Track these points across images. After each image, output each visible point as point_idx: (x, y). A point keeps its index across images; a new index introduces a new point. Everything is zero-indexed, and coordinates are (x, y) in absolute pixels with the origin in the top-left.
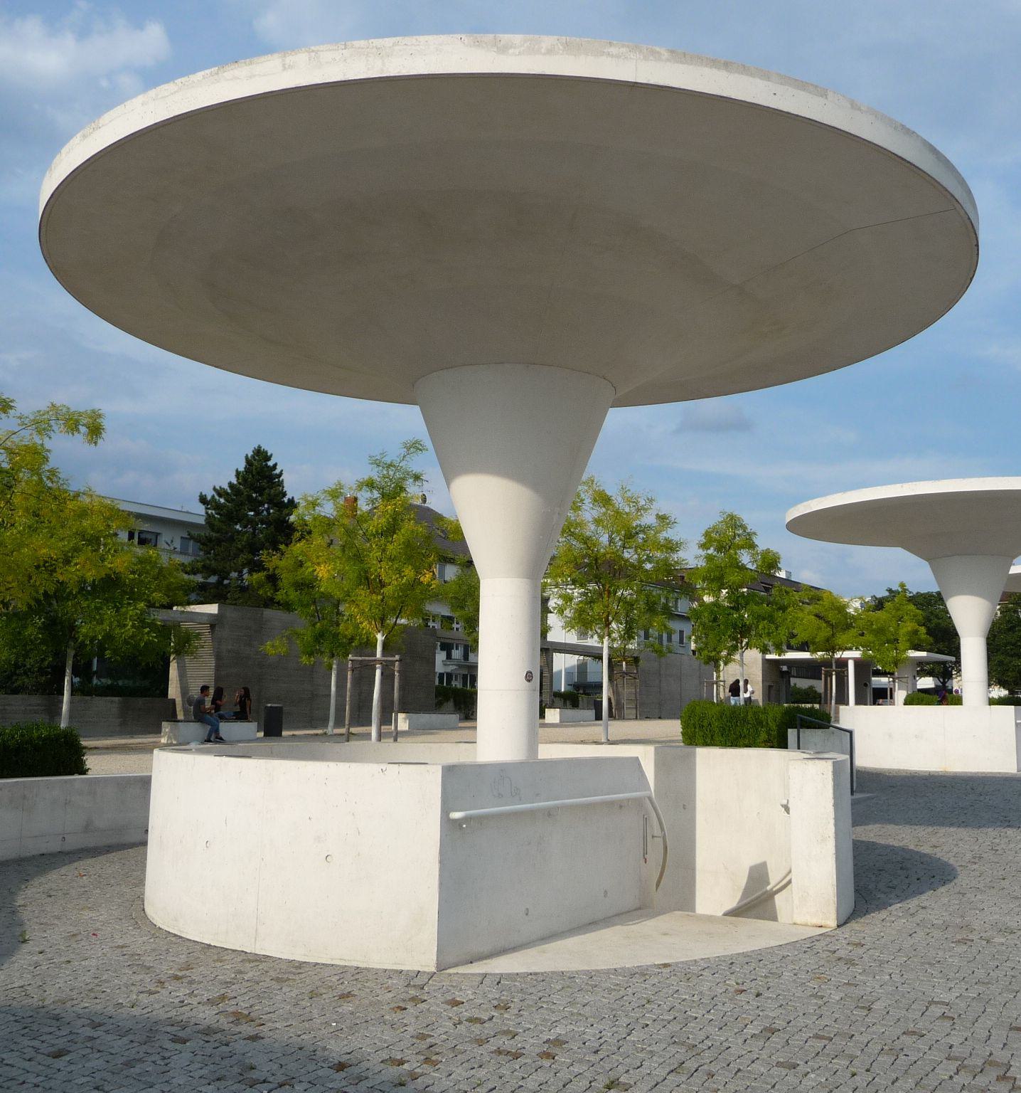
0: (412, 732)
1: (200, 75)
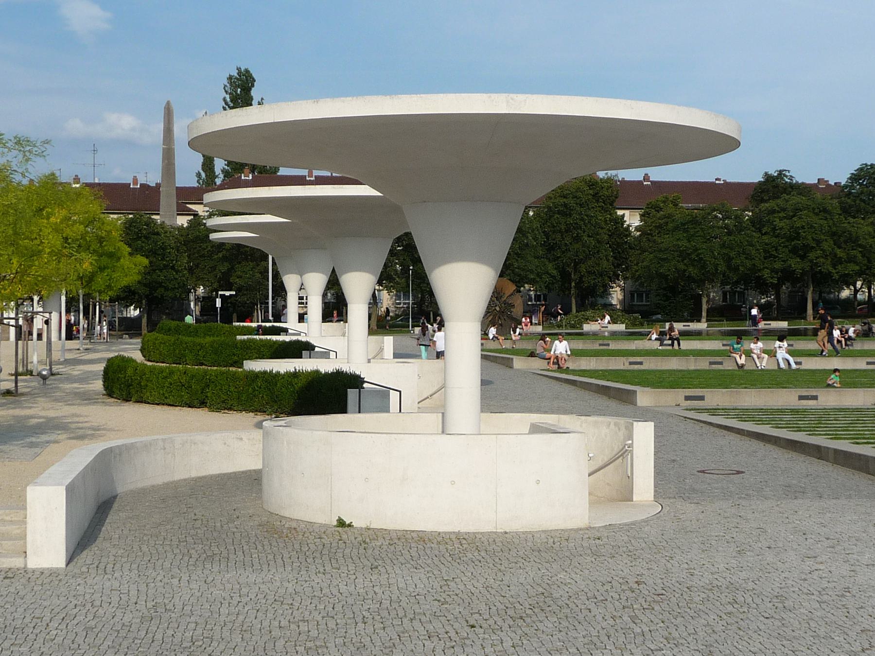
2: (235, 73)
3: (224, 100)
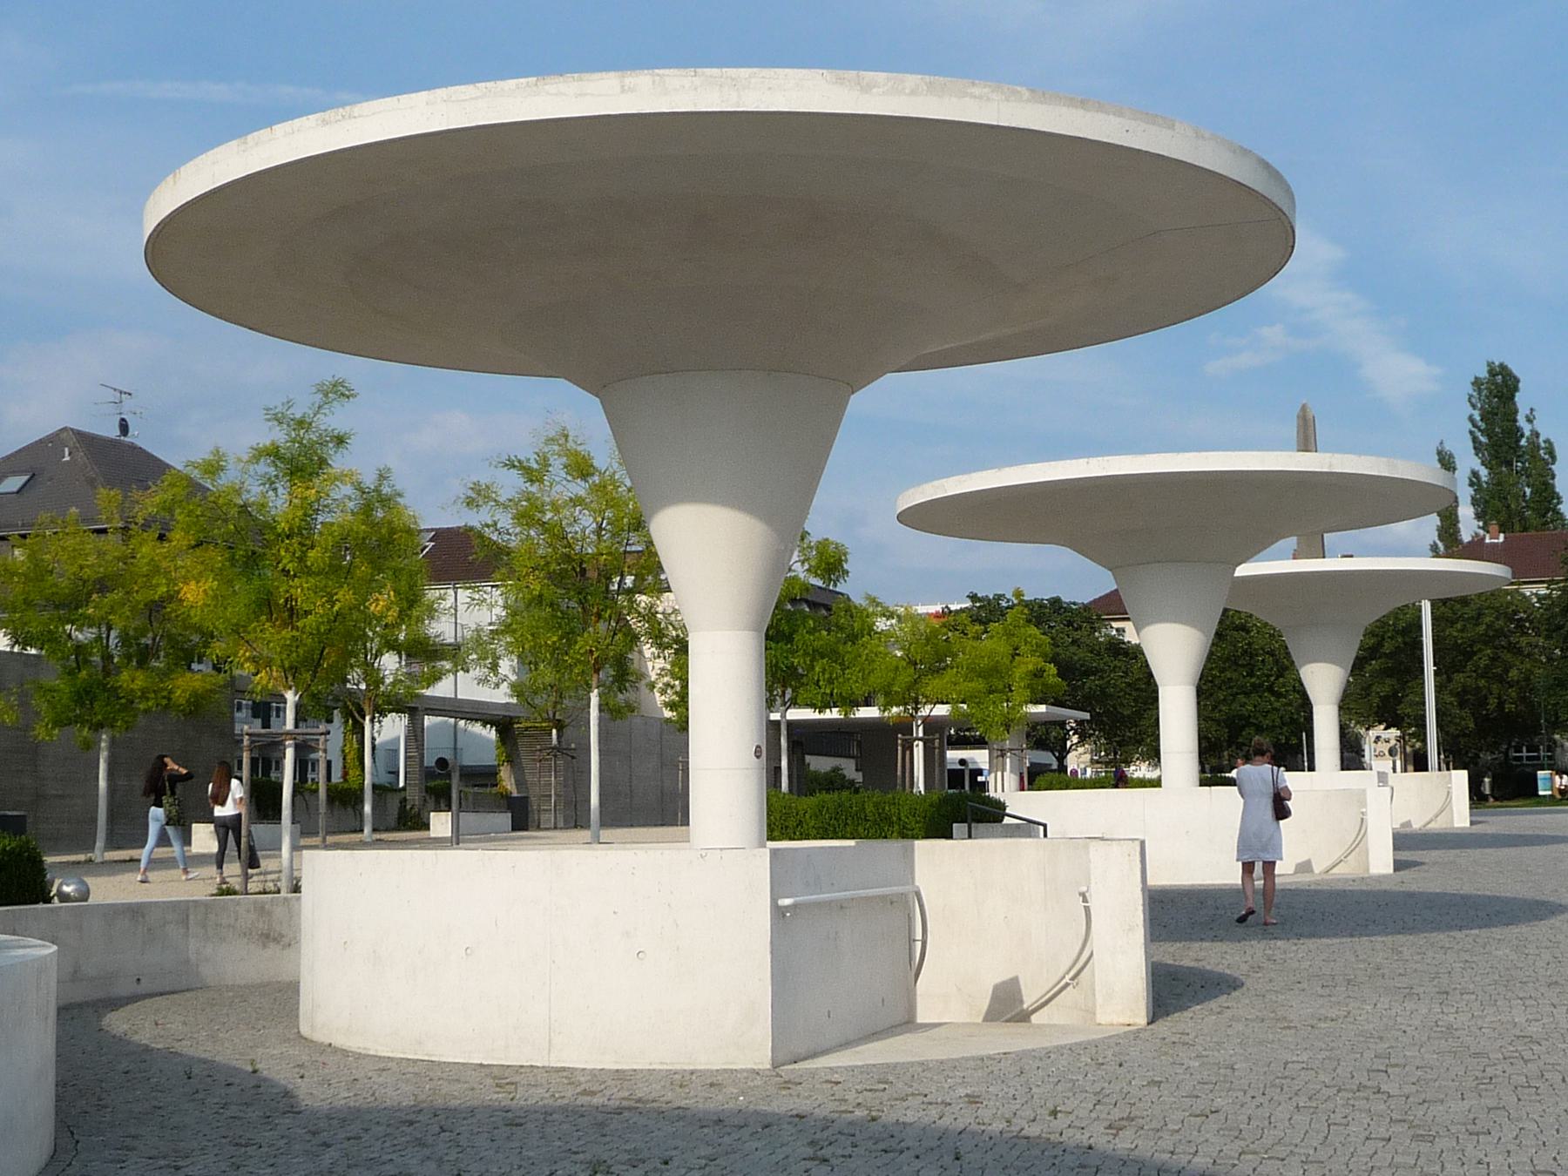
0: (456, 839)
1: (512, 83)
2: (1483, 373)
3: (1471, 419)
